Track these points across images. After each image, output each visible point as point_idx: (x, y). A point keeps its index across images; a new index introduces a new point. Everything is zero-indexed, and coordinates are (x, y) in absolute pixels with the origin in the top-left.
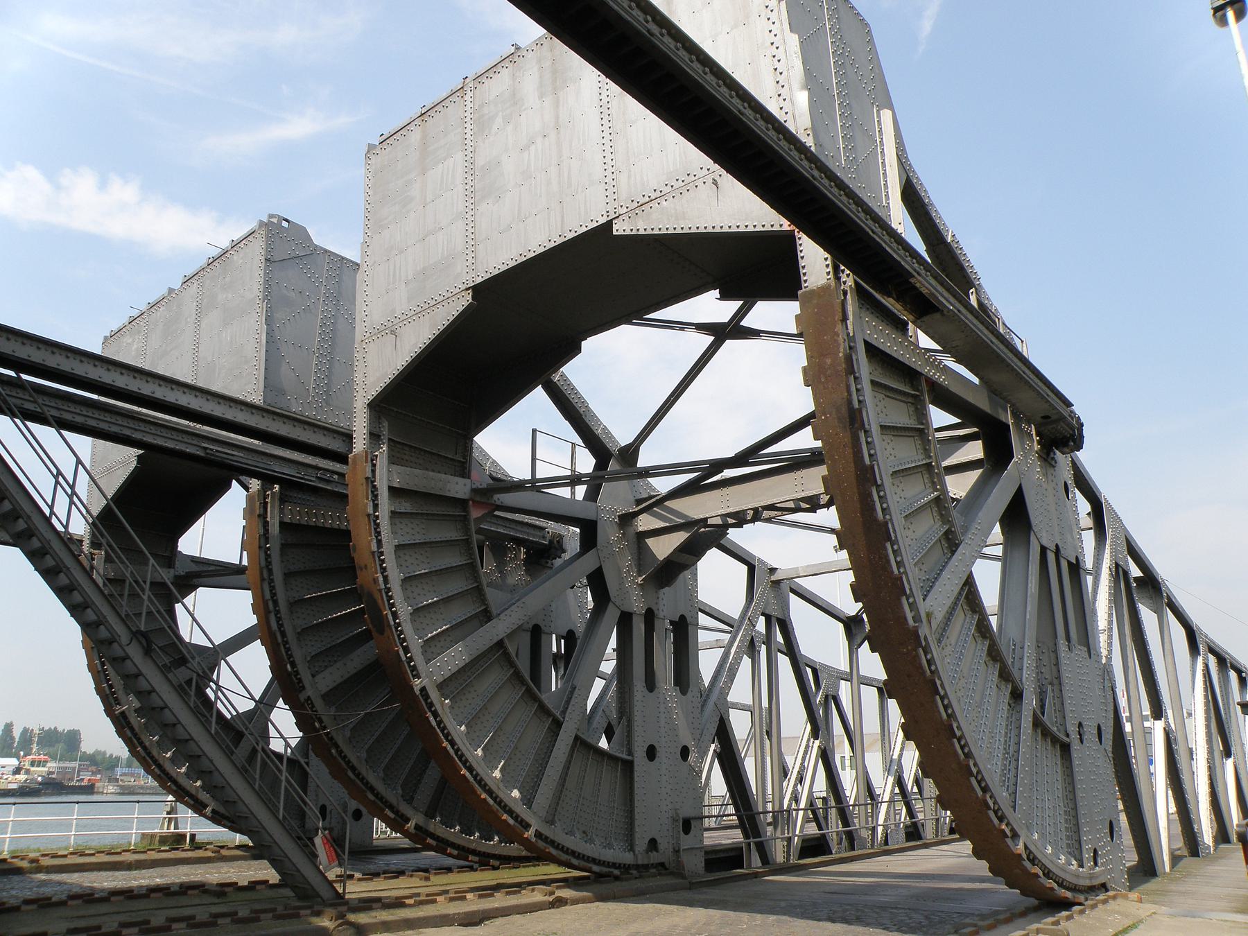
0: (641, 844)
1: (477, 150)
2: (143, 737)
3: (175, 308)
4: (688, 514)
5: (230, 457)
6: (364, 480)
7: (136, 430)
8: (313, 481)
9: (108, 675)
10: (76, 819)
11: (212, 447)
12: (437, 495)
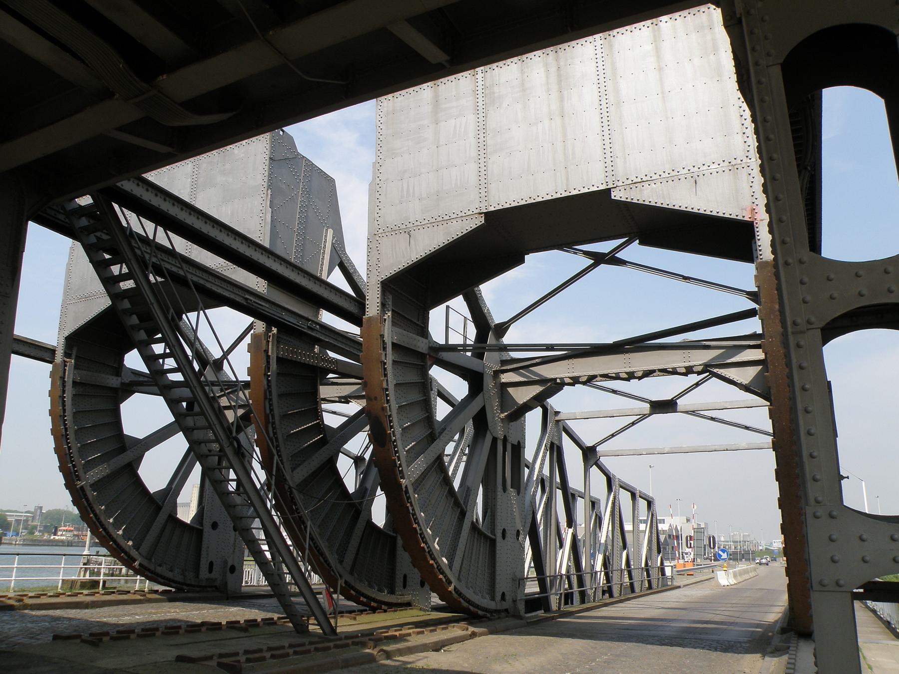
0: (498, 596)
1: (489, 115)
2: (95, 507)
3: (166, 180)
4: (541, 374)
5: (259, 306)
6: (379, 336)
7: (207, 281)
8: (305, 329)
9: (72, 457)
10: (63, 567)
11: (251, 298)
12: (412, 349)
